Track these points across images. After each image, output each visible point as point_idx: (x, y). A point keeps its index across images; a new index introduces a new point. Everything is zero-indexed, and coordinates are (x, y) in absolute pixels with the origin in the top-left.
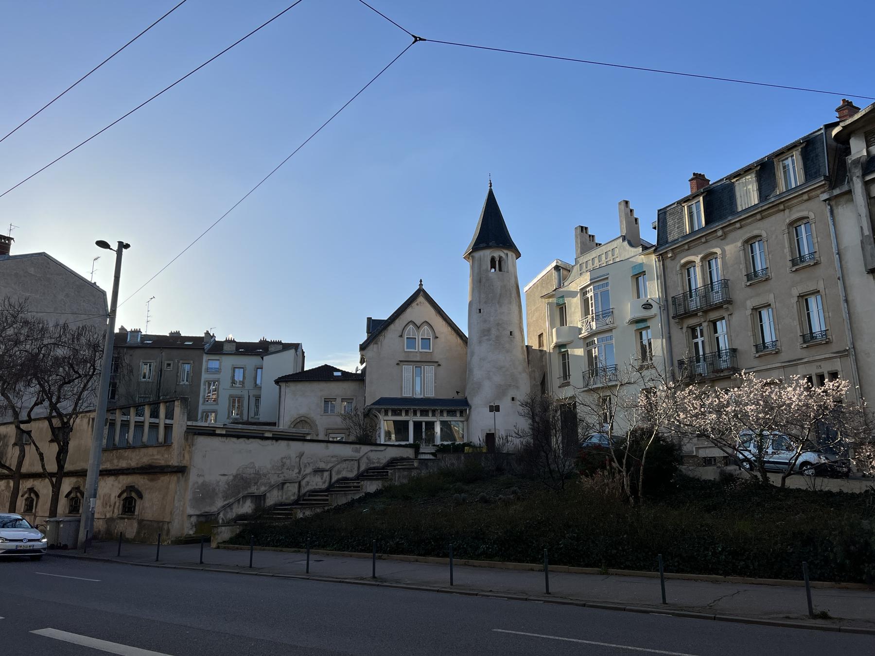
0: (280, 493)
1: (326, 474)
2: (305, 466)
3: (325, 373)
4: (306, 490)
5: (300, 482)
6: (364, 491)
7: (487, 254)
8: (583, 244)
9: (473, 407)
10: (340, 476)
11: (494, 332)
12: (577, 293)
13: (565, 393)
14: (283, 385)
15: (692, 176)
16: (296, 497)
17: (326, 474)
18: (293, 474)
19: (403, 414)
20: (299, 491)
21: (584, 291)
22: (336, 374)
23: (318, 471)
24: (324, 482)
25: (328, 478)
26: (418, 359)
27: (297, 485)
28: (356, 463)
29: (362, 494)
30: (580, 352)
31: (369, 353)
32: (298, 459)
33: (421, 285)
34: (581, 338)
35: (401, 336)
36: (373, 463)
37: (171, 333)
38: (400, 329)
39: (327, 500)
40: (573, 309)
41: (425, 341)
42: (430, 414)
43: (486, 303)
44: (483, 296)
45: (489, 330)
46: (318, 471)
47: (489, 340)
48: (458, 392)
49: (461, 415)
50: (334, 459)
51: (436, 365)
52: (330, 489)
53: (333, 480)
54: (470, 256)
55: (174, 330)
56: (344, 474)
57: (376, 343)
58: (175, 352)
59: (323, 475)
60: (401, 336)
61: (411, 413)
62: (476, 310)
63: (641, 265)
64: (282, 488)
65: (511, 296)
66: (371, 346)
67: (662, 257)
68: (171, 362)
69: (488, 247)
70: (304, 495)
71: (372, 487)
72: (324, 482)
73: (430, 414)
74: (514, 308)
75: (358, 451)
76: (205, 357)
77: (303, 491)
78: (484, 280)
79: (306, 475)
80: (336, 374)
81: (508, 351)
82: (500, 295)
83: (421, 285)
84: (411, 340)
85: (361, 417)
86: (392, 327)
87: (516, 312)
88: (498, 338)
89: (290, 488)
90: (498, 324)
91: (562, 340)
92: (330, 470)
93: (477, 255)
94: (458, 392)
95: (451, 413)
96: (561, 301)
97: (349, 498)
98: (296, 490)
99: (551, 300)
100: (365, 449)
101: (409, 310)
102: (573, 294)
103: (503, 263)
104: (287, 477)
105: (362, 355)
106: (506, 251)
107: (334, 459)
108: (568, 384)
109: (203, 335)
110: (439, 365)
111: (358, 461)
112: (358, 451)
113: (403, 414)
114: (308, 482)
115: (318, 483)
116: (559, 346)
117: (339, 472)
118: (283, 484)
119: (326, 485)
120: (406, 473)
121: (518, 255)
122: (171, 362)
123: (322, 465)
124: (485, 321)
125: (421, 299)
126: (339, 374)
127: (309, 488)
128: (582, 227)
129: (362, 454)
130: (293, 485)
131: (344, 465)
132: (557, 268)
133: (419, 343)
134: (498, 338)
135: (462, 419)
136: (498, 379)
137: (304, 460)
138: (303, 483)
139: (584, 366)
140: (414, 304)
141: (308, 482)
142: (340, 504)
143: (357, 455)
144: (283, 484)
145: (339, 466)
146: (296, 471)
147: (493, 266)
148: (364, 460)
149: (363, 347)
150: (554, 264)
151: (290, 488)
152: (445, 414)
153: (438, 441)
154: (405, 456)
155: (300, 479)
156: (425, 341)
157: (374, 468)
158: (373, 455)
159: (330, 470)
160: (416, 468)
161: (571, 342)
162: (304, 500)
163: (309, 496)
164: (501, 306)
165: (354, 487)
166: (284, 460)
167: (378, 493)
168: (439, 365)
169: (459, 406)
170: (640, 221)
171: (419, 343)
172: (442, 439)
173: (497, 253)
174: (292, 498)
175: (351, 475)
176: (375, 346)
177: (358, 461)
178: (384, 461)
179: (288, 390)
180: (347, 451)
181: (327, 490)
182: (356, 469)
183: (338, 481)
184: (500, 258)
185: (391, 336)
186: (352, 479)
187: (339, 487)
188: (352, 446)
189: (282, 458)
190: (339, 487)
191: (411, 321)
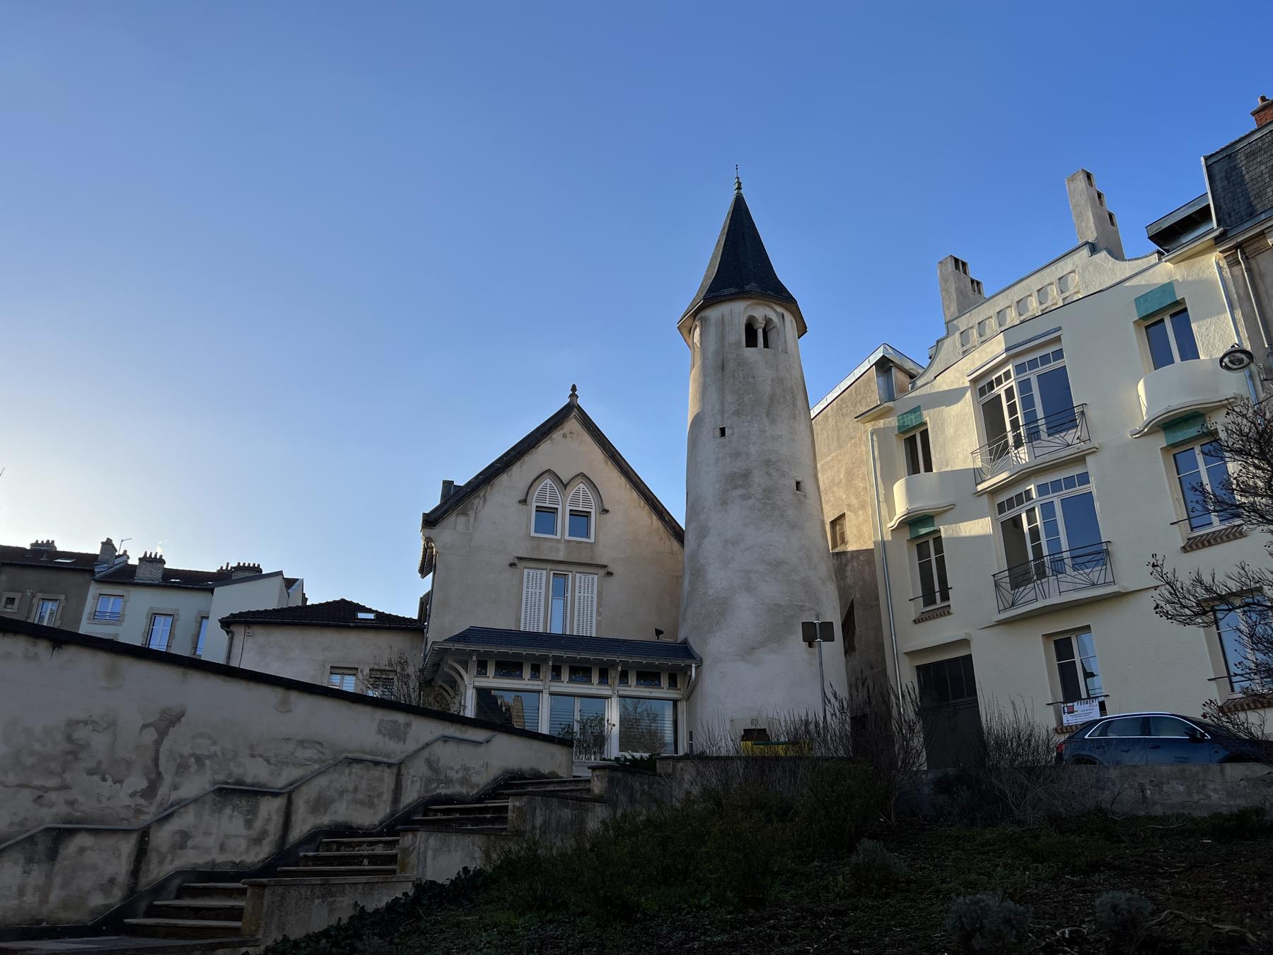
0: (37, 875)
1: (270, 809)
2: (182, 769)
3: (341, 615)
4: (169, 868)
5: (144, 833)
6: (413, 874)
7: (737, 312)
8: (961, 293)
9: (706, 663)
10: (325, 820)
11: (758, 479)
12: (964, 390)
13: (941, 632)
14: (239, 631)
15: (1260, 103)
16: (116, 897)
17: (270, 809)
18: (120, 797)
19: (527, 673)
20: (135, 873)
21: (983, 384)
22: (361, 615)
23: (237, 793)
24: (257, 841)
25: (277, 820)
26: (561, 556)
27: (127, 846)
28: (388, 777)
29: (402, 890)
30: (982, 526)
31: (446, 534)
32: (150, 736)
33: (573, 395)
34: (984, 492)
35: (524, 502)
36: (449, 781)
37: (32, 545)
38: (523, 485)
39: (235, 913)
40: (950, 431)
41: (580, 516)
42: (595, 679)
43: (737, 413)
44: (730, 398)
45: (746, 475)
46: (237, 793)
47: (745, 497)
48: (659, 632)
49: (673, 684)
50: (310, 753)
51: (602, 572)
52: (284, 865)
53: (296, 834)
54: (685, 328)
55: (42, 538)
56: (342, 812)
57: (464, 513)
58: (30, 576)
59: (253, 811)
60: (524, 502)
61: (546, 672)
62: (712, 432)
63: (1168, 287)
64: (52, 856)
65: (794, 404)
66: (452, 519)
67: (1243, 252)
68: (17, 596)
69: (741, 295)
70: (159, 888)
71: (444, 859)
72: (257, 841)
73: (595, 679)
74: (802, 427)
75: (398, 734)
76: (94, 590)
77: (156, 871)
78: (731, 365)
79: (182, 804)
80: (361, 615)
81: (793, 526)
82: (772, 398)
83: (573, 395)
84: (547, 514)
85: (414, 683)
86: (504, 479)
87: (808, 441)
88: (769, 492)
89: (91, 857)
90: (768, 463)
91: (926, 504)
92: (288, 794)
93: (714, 313)
94: (659, 632)
95: (648, 676)
96: (912, 420)
97: (344, 908)
98: (121, 868)
99: (881, 423)
100: (424, 730)
101: (545, 447)
102: (953, 396)
103: (772, 336)
104: (87, 806)
105: (428, 540)
106: (780, 309)
107: (310, 753)
108: (946, 611)
109: (96, 550)
110: (610, 574)
111: (398, 768)
112: (398, 734)
113: (527, 673)
114: (185, 836)
115: (230, 839)
116: (913, 522)
117: (320, 805)
118: (59, 835)
119: (263, 852)
120: (567, 813)
121: (802, 330)
122: (17, 596)
123: (256, 772)
124: (736, 455)
125: (573, 425)
126: (371, 616)
127: (191, 858)
128: (956, 260)
129: (411, 746)
130: (111, 841)
131: (345, 778)
132: (884, 366)
133: (563, 521)
134: (769, 492)
135: (673, 694)
136: (771, 590)
137: (179, 741)
138: (162, 837)
139: (997, 560)
140: (557, 435)
141: (185, 836)
142: (296, 933)
143: (396, 749)
144: (59, 835)
145: (323, 781)
146: (138, 782)
147: (751, 340)
148: (418, 769)
149: (431, 521)
150: (878, 355)
151: (91, 857)
152: (632, 680)
153: (613, 750)
154: (545, 769)
155: (146, 819)
156: (580, 516)
157: (449, 799)
158: (449, 756)
159: (288, 794)
160: (599, 799)
161: (952, 507)
162: (152, 911)
163: (182, 892)
164: (773, 422)
165: (374, 859)
166: (81, 734)
167: (467, 887)
168: (610, 574)
169: (666, 662)
170: (1116, 219)
171: (563, 521)
172: (623, 747)
173: (761, 312)
174: (97, 900)
175: (368, 818)
176: (462, 519)
177: (398, 768)
178: (482, 779)
179: (249, 643)
180: (361, 730)
181: (267, 868)
182: (387, 796)
183: (313, 837)
184: (768, 321)
185: (500, 504)
186: (367, 834)
187: (316, 860)
188: (380, 715)
189: (72, 724)
190: (316, 860)
191: (548, 471)
